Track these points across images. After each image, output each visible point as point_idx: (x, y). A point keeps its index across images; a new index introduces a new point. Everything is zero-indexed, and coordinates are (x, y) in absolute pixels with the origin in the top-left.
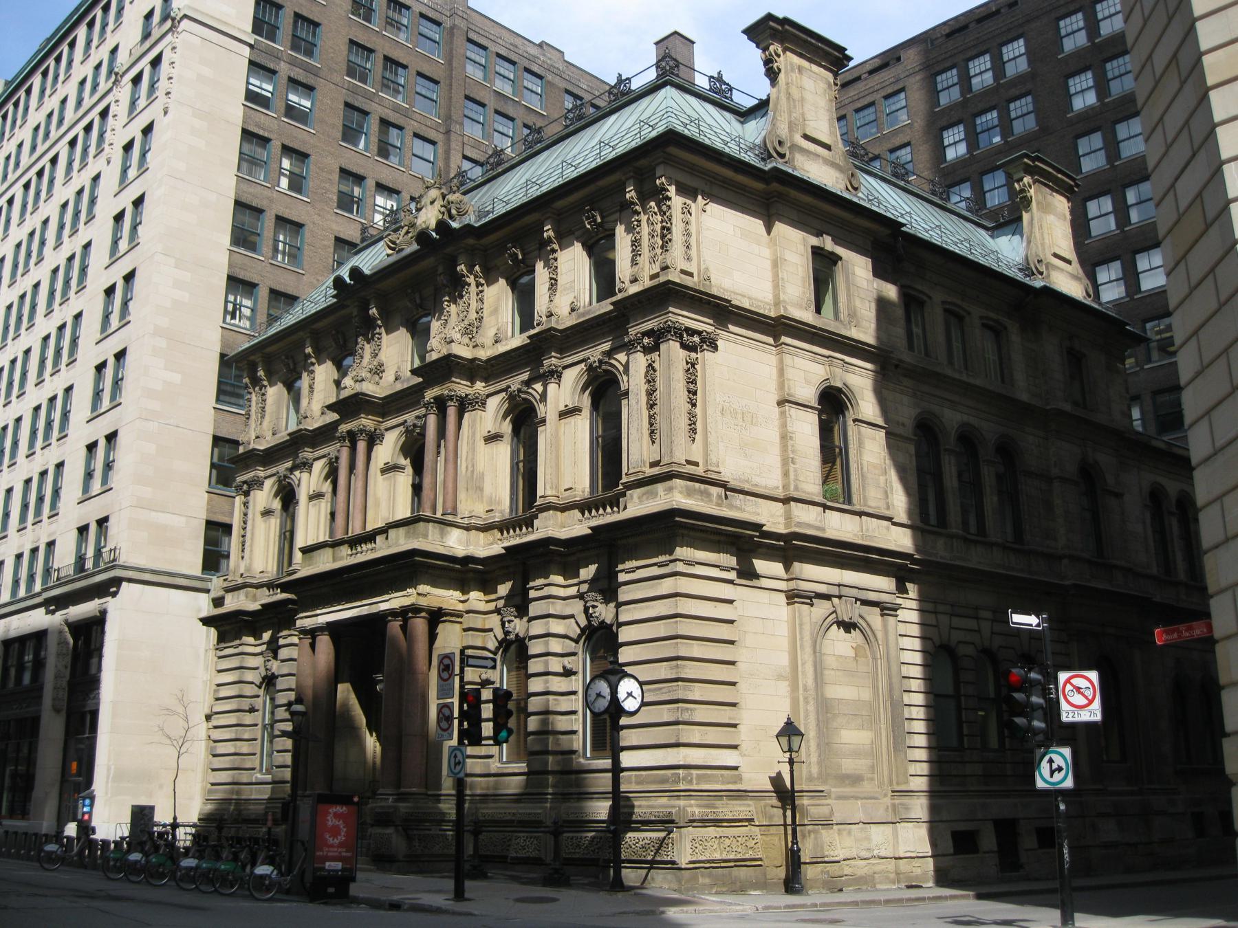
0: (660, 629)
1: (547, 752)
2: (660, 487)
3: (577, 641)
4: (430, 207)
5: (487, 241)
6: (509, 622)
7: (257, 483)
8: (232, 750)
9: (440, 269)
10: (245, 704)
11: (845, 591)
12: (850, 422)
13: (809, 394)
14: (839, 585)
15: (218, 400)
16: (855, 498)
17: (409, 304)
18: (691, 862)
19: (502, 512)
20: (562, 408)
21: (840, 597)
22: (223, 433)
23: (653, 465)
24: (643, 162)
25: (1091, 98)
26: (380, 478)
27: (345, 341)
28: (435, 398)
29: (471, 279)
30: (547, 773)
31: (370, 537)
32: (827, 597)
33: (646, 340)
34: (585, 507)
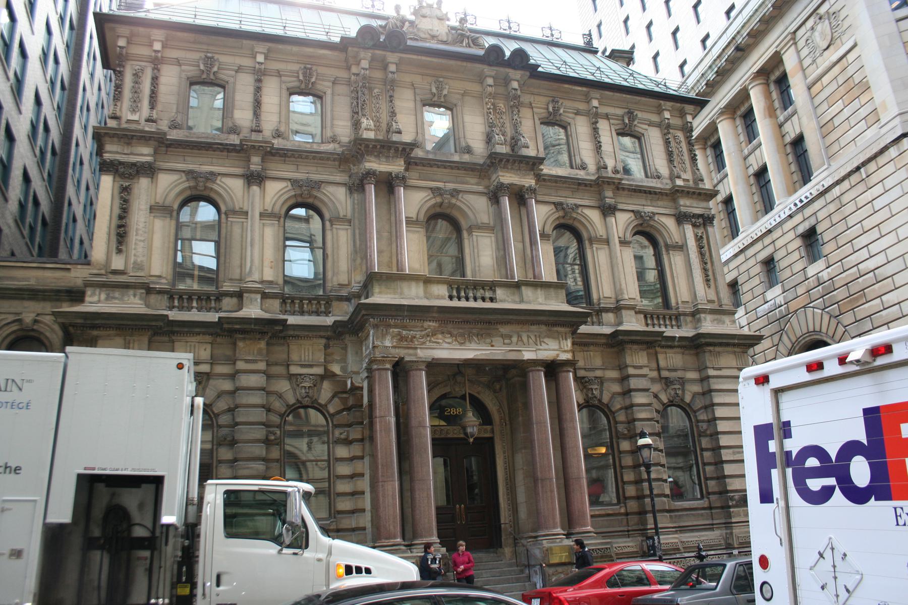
7: (149, 170)
31: (720, 369)
33: (693, 220)
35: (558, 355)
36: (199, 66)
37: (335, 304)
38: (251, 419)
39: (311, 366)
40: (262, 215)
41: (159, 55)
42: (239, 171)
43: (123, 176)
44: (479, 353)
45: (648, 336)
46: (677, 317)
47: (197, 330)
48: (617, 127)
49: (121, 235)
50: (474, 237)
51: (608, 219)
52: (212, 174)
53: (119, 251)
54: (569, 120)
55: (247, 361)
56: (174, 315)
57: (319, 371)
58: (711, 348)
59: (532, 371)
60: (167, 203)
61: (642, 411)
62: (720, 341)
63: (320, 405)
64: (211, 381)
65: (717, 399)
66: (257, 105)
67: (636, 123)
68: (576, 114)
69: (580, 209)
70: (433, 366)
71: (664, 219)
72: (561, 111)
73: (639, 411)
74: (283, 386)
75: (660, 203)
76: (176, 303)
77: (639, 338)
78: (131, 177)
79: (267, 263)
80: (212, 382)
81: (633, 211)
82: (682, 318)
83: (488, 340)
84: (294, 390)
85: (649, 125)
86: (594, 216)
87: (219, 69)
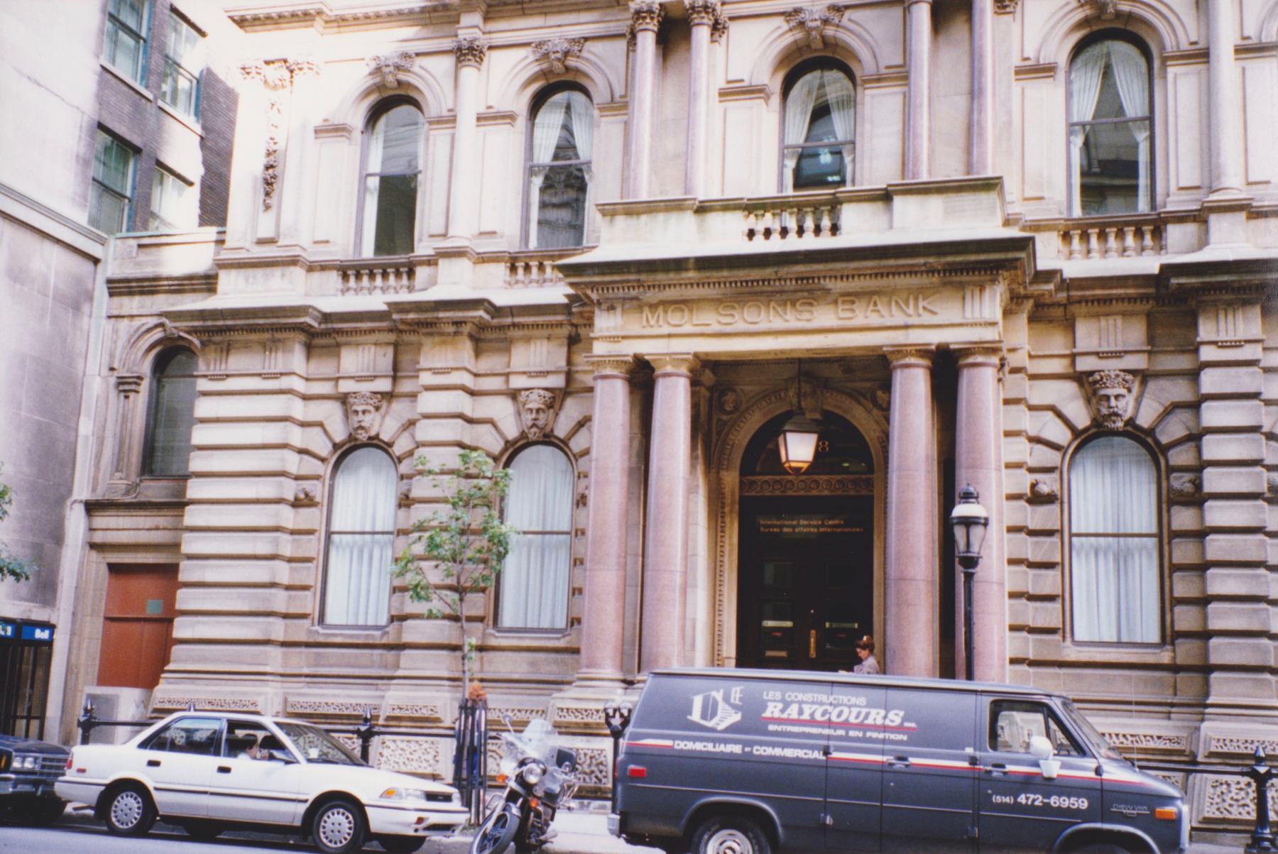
3: (323, 460)
6: (1117, 397)
8: (265, 578)
10: (290, 489)
20: (482, 110)
23: (261, 242)
26: (718, 107)
34: (350, 271)
50: (1170, 76)
55: (436, 372)
57: (558, 381)
80: (570, 402)
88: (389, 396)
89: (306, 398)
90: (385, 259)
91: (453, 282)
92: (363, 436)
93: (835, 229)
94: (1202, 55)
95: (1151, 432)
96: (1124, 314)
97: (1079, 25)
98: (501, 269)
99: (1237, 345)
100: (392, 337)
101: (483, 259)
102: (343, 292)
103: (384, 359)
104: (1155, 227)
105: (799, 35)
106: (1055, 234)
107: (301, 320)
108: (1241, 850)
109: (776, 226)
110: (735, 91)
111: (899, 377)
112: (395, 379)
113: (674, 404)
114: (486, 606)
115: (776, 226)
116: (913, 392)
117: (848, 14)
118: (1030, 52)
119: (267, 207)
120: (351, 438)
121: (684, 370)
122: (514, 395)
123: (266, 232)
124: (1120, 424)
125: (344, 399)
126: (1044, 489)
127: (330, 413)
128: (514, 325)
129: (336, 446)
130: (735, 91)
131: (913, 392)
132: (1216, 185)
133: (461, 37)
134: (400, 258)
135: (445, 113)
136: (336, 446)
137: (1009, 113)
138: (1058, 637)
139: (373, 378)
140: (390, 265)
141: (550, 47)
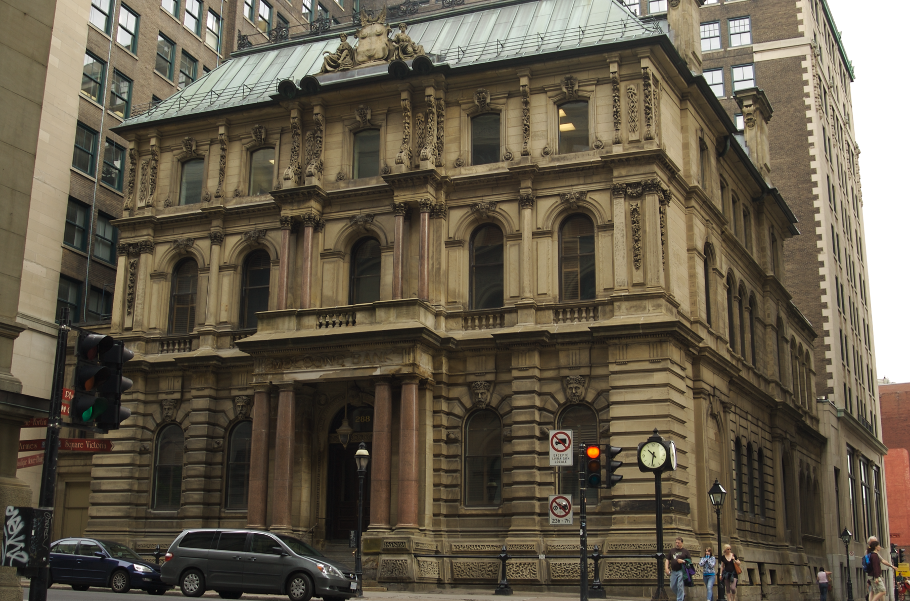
0: (653, 409)
1: (533, 498)
2: (649, 304)
4: (374, 38)
5: (452, 80)
7: (149, 248)
9: (404, 95)
11: (717, 393)
12: (711, 270)
13: (700, 245)
14: (714, 388)
15: (74, 164)
16: (713, 325)
17: (358, 118)
18: (610, 552)
19: (463, 304)
21: (714, 396)
22: (75, 196)
24: (628, 52)
25: (716, 44)
27: (266, 135)
28: (406, 203)
29: (434, 110)
30: (533, 514)
31: (625, 363)
32: (709, 395)
33: (629, 191)
34: (559, 311)
35: (400, 369)
36: (473, 102)
37: (507, 316)
38: (198, 433)
39: (246, 389)
40: (221, 269)
41: (616, 75)
42: (205, 234)
43: (632, 197)
44: (321, 374)
45: (646, 329)
46: (595, 308)
47: (169, 368)
48: (555, 99)
49: (130, 302)
51: (615, 201)
52: (189, 240)
53: (129, 313)
54: (500, 107)
55: (198, 389)
56: (555, 328)
58: (616, 341)
59: (407, 384)
60: (161, 270)
61: (522, 413)
62: (619, 333)
63: (234, 420)
64: (497, 388)
65: (615, 397)
66: (222, 172)
67: (576, 88)
68: (508, 98)
69: (589, 195)
70: (300, 387)
71: (597, 197)
72: (488, 101)
73: (518, 414)
74: (228, 406)
75: (596, 178)
76: (469, 324)
77: (518, 340)
78: (640, 196)
79: (223, 308)
80: (183, 406)
81: (558, 195)
82: (600, 308)
83: (340, 361)
84: (564, 390)
85: (596, 85)
86: (510, 209)
87: (197, 146)
88: (590, 377)
89: (540, 380)
90: (175, 335)
91: (526, 324)
92: (168, 420)
93: (354, 323)
94: (518, 236)
95: (496, 409)
96: (648, 343)
97: (472, 222)
98: (550, 314)
99: (527, 369)
100: (180, 373)
101: (539, 309)
102: (162, 352)
103: (178, 385)
104: (594, 309)
105: (354, 228)
106: (460, 319)
107: (674, 329)
108: (579, 599)
109: (344, 320)
110: (326, 255)
111: (282, 395)
112: (496, 373)
113: (286, 404)
114: (221, 497)
115: (344, 320)
116: (382, 395)
117: (499, 206)
118: (451, 235)
119: (637, 268)
120: (164, 420)
121: (291, 388)
122: (233, 399)
123: (128, 324)
124: (484, 406)
125: (563, 379)
126: (452, 436)
127: (154, 409)
128: (233, 366)
129: (158, 425)
130: (326, 255)
131: (382, 395)
132: (522, 296)
133: (615, 183)
134: (589, 302)
135: (515, 232)
136: (158, 425)
137: (440, 264)
138: (458, 504)
139: (173, 393)
140: (583, 306)
141: (568, 196)
